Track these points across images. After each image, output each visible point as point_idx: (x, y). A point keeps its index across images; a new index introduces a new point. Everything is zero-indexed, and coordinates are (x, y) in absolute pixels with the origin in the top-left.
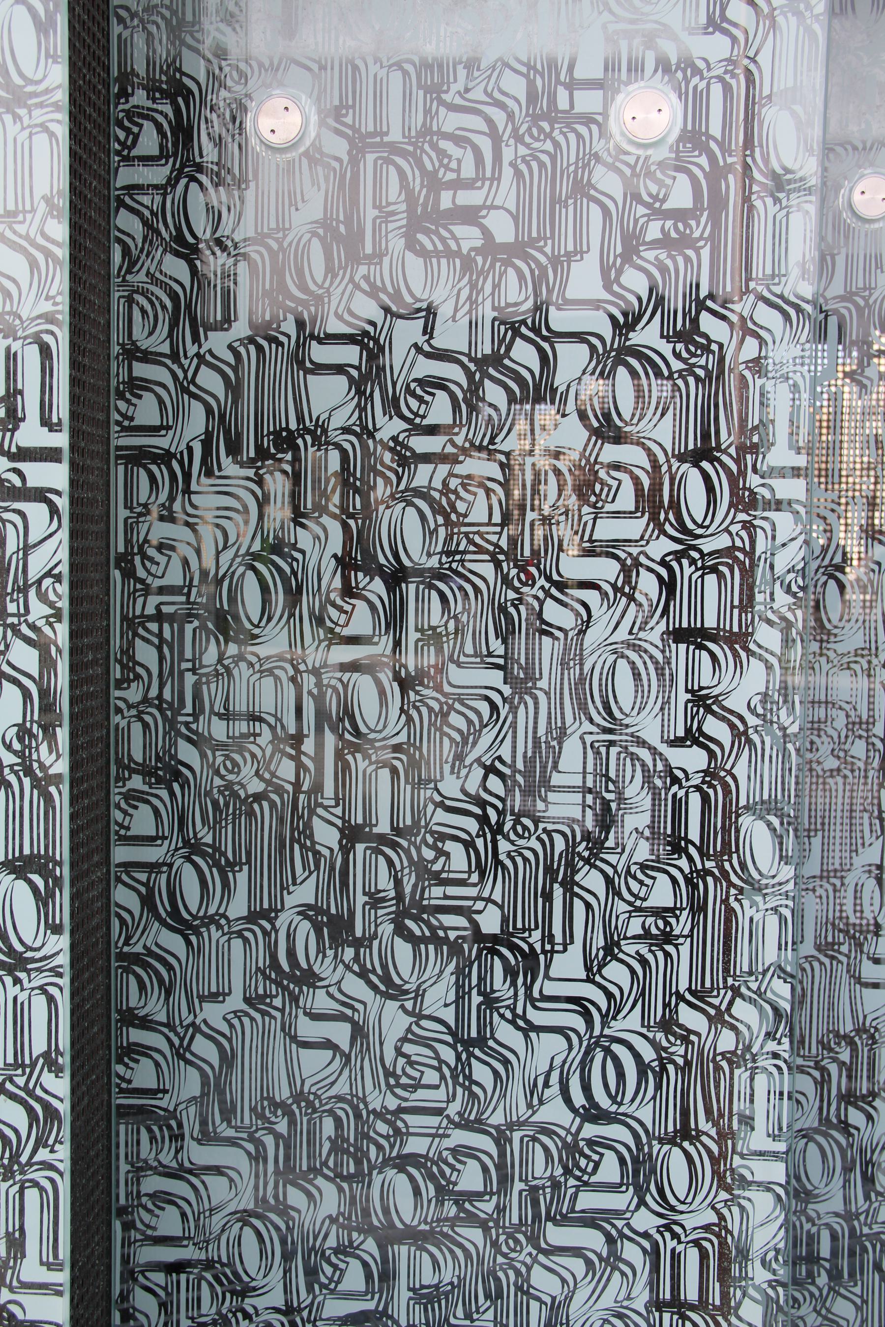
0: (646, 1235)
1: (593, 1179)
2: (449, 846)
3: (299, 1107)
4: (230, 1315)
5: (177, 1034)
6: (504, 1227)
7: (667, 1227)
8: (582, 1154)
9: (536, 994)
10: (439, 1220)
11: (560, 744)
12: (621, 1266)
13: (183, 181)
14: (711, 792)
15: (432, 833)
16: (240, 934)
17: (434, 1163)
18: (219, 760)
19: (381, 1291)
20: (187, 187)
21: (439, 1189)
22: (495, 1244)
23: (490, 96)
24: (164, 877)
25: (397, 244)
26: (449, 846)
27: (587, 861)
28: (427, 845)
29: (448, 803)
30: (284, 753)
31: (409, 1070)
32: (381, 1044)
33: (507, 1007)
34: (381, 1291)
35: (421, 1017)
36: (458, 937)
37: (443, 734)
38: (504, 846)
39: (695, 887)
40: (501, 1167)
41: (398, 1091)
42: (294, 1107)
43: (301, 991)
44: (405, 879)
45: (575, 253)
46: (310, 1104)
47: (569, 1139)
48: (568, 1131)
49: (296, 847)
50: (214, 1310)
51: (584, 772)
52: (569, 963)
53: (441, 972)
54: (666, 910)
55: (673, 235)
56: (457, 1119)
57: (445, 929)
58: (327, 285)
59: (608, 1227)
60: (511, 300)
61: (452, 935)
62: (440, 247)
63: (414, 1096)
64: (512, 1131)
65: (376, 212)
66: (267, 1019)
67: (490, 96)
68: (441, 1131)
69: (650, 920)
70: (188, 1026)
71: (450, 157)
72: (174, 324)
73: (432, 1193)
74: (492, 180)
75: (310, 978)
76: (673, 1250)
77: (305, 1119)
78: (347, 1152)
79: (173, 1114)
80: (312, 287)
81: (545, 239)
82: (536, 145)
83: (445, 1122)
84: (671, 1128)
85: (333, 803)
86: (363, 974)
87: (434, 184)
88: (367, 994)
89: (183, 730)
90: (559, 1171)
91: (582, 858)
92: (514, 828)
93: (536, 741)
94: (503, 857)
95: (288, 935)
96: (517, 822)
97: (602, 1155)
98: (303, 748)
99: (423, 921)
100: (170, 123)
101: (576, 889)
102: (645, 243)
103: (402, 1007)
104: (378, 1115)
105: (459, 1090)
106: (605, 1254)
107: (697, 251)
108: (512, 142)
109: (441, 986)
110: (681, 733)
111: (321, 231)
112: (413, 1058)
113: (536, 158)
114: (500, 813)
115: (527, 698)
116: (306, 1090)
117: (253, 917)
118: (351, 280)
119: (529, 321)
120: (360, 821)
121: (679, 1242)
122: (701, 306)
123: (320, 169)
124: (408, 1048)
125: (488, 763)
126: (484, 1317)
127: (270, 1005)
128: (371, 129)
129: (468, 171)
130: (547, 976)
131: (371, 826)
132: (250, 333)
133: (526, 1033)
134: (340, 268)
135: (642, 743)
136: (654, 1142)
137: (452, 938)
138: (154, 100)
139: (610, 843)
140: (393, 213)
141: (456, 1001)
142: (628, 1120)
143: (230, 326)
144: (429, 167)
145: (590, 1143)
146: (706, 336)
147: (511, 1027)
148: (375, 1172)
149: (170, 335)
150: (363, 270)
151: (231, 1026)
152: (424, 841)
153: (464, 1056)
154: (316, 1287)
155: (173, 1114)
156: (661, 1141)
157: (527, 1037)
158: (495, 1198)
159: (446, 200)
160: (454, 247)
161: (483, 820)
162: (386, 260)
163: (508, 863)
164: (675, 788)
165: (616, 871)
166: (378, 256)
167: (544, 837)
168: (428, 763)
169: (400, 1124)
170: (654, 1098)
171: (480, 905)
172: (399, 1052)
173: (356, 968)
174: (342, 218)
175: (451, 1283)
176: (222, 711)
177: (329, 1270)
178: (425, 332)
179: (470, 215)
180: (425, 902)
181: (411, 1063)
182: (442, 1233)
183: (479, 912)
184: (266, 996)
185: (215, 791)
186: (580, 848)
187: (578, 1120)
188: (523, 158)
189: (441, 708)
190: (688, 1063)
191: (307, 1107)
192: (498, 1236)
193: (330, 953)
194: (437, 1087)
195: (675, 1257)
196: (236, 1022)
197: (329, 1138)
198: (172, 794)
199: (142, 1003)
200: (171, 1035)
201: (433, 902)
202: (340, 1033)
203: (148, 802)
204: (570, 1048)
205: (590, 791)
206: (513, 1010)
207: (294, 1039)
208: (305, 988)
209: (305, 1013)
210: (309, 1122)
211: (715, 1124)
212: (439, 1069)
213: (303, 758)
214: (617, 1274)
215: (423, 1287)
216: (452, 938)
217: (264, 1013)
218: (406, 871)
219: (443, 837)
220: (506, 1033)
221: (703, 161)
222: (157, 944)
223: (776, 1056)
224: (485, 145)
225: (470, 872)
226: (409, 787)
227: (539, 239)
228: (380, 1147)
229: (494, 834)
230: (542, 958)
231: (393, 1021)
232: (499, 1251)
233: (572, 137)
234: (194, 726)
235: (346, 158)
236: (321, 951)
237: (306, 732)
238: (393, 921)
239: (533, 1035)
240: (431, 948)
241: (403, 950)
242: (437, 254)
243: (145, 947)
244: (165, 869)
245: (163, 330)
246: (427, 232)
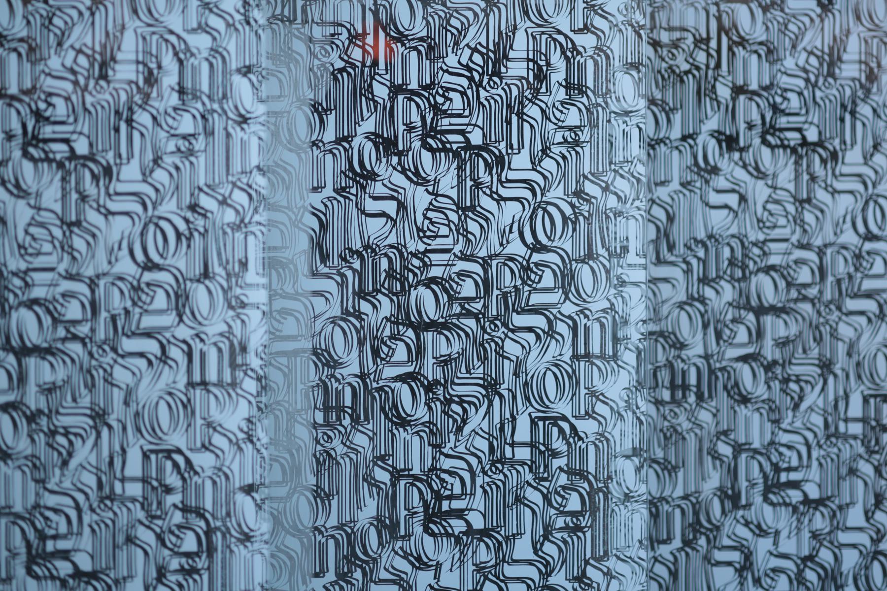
0: (570, 317)
1: (539, 286)
2: (452, 95)
3: (367, 253)
4: (327, 380)
5: (294, 213)
6: (488, 317)
7: (582, 311)
8: (532, 271)
9: (503, 179)
10: (450, 316)
11: (514, 34)
12: (556, 336)
13: (296, 495)
14: (599, 58)
15: (442, 87)
16: (330, 151)
17: (446, 281)
18: (317, 49)
19: (417, 360)
20: (298, 498)
21: (450, 298)
22: (483, 328)
23: (469, 450)
24: (285, 120)
25: (418, 529)
26: (452, 95)
27: (530, 101)
28: (440, 95)
29: (450, 70)
30: (356, 45)
31: (431, 227)
32: (415, 213)
33: (487, 187)
34: (417, 360)
35: (437, 195)
36: (458, 147)
37: (447, 30)
38: (818, 94)
39: (592, 113)
40: (486, 281)
41: (425, 240)
42: (364, 253)
43: (367, 183)
44: (427, 115)
45: (518, 534)
46: (373, 251)
47: (525, 263)
48: (524, 258)
49: (363, 98)
50: (317, 378)
51: (528, 50)
52: (521, 160)
53: (449, 168)
54: (576, 127)
55: (571, 525)
56: (459, 255)
57: (450, 143)
58: (379, 552)
59: (548, 313)
60: (482, 560)
61: (455, 146)
62: (443, 531)
63: (434, 242)
64: (491, 260)
65: (406, 512)
66: (347, 201)
67: (469, 450)
68: (450, 263)
69: (568, 519)
70: (300, 208)
71: (447, 482)
72: (291, 574)
73: (446, 299)
74: (471, 494)
75: (372, 176)
76: (585, 325)
77: (370, 260)
78: (397, 279)
79: (291, 261)
80: (371, 553)
81: (501, 527)
82: (494, 476)
83: (453, 257)
84: (582, 254)
85: (384, 72)
86: (403, 172)
87: (438, 497)
88: (406, 183)
89: (296, 33)
90: (519, 282)
91: (528, 99)
92: (488, 83)
93: (500, 33)
94: (483, 100)
95: (359, 151)
96: (490, 79)
97: (543, 271)
98: (367, 41)
99: (437, 139)
100: (288, 463)
101: (525, 117)
102: (555, 529)
103: (427, 190)
104: (414, 255)
105: (461, 237)
106: (546, 330)
107: (584, 533)
108: (481, 474)
109: (449, 176)
110: (581, 26)
111: (375, 523)
112: (434, 220)
113: (495, 483)
114: (481, 75)
115: (494, 8)
116: (371, 242)
117: (338, 141)
118: (393, 549)
119: (493, 572)
120: (400, 82)
121: (589, 320)
122: (587, 563)
123: (374, 489)
124: (430, 214)
125: (473, 46)
126: (478, 371)
127: (349, 193)
128: (402, 467)
129: (457, 490)
130: (509, 168)
131: (407, 85)
132: (335, 579)
133: (498, 202)
134: (387, 542)
135: (559, 32)
136: (573, 262)
137: (454, 148)
138: (277, 66)
139: (543, 90)
140: (416, 513)
141: (458, 185)
142: (558, 250)
143: (324, 576)
144: (435, 488)
145: (537, 265)
146: (589, 579)
147: (490, 199)
148: (412, 289)
149: (289, 580)
150: (399, 544)
151: (326, 206)
152: (437, 92)
153: (463, 217)
154: (379, 360)
155: (291, 261)
156: (576, 260)
157: (498, 203)
158: (482, 300)
159: (445, 506)
160: (450, 531)
161: (471, 79)
162: (412, 538)
163: (486, 103)
164: (579, 57)
165: (547, 106)
166: (408, 536)
167: (506, 87)
168: (441, 435)
169: (426, 259)
170: (572, 236)
171: (470, 128)
172: (425, 217)
173: (399, 168)
174: (387, 515)
175: (458, 353)
176: (319, 21)
177: (385, 349)
178: (435, 578)
179: (459, 514)
180: (439, 128)
181: (432, 223)
182: (452, 323)
183: (470, 132)
184: (346, 187)
185: (315, 68)
186: (526, 94)
187: (529, 251)
188: (488, 483)
189: (446, 16)
190: (591, 215)
191: (372, 253)
192: (485, 322)
193: (384, 160)
194: (447, 236)
195: (587, 329)
196: (329, 204)
197: (385, 270)
198: (289, 70)
199: (272, 195)
200: (290, 213)
201: (443, 128)
202: (390, 207)
203: (277, 227)
204: (524, 210)
205: (532, 60)
206: (491, 189)
207: (363, 212)
208: (369, 182)
209: (370, 197)
210: (373, 260)
211: (608, 250)
212: (449, 226)
213: (367, 47)
214: (554, 341)
215: (441, 356)
216: (454, 148)
217: (345, 197)
218: (428, 110)
219: (448, 89)
220: (486, 202)
221: (586, 485)
222: (281, 160)
223: (639, 209)
224: (467, 476)
225: (464, 110)
226: (428, 62)
227: (498, 527)
228: (415, 275)
229: (477, 87)
230: (506, 157)
231: (421, 198)
232: (485, 331)
233: (514, 472)
234: (302, 30)
235: (389, 483)
236: (378, 159)
237: (368, 32)
238: (421, 140)
239: (502, 203)
240: (443, 154)
241: (426, 156)
242: (441, 535)
243: (274, 161)
244: (285, 114)
245: (285, 577)
246: (435, 523)
